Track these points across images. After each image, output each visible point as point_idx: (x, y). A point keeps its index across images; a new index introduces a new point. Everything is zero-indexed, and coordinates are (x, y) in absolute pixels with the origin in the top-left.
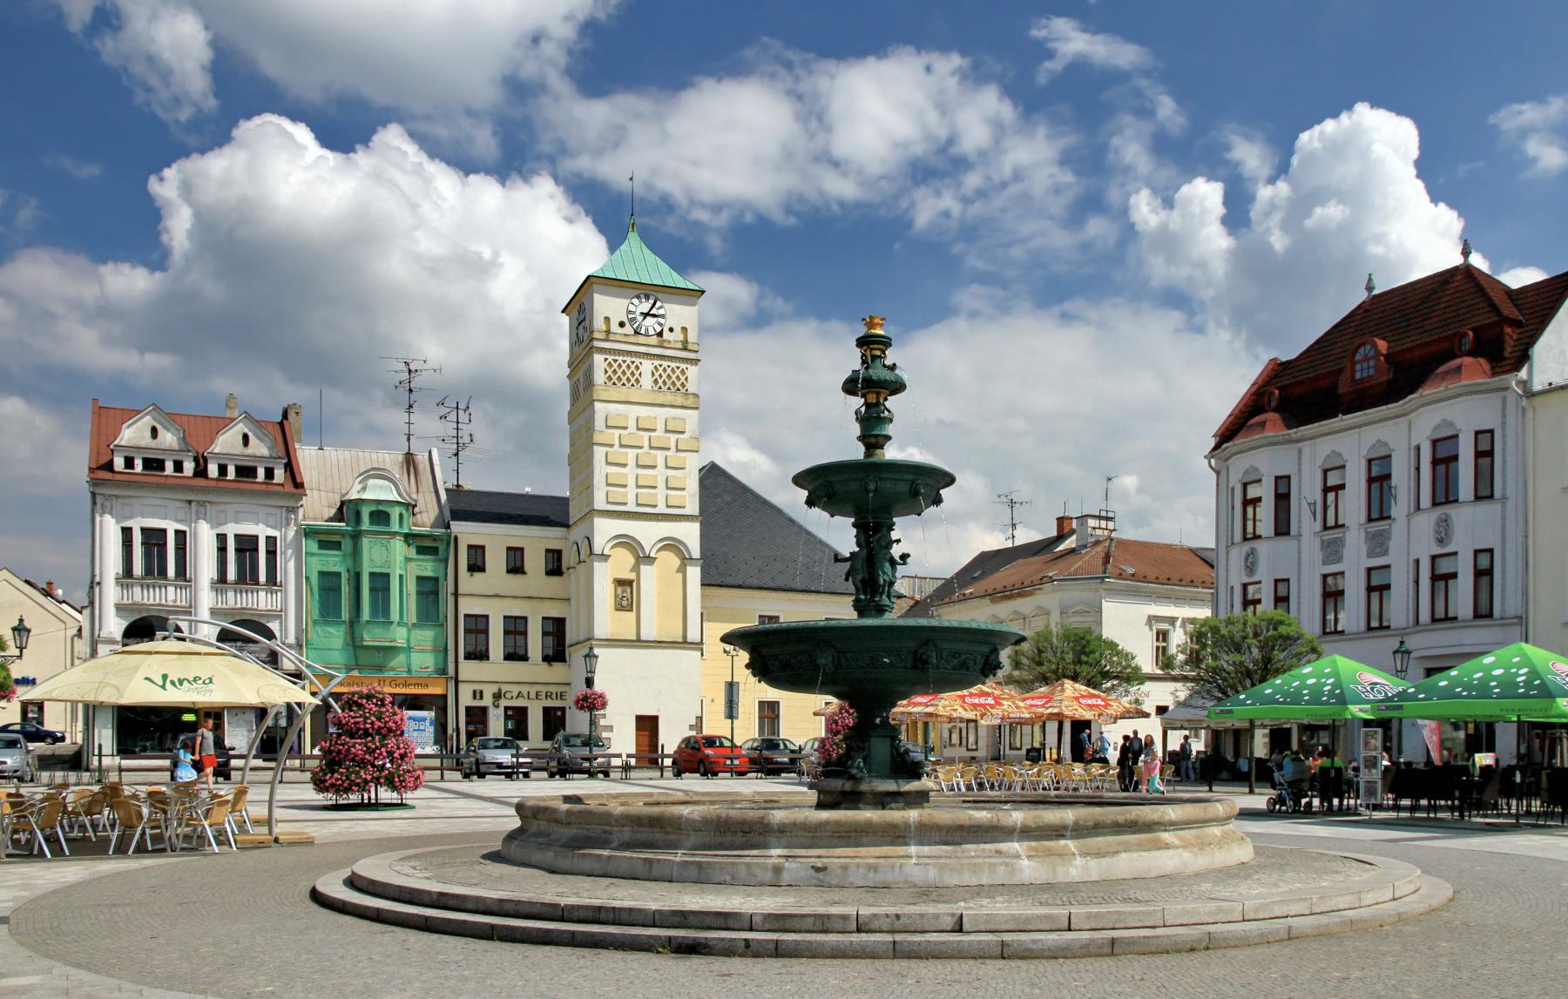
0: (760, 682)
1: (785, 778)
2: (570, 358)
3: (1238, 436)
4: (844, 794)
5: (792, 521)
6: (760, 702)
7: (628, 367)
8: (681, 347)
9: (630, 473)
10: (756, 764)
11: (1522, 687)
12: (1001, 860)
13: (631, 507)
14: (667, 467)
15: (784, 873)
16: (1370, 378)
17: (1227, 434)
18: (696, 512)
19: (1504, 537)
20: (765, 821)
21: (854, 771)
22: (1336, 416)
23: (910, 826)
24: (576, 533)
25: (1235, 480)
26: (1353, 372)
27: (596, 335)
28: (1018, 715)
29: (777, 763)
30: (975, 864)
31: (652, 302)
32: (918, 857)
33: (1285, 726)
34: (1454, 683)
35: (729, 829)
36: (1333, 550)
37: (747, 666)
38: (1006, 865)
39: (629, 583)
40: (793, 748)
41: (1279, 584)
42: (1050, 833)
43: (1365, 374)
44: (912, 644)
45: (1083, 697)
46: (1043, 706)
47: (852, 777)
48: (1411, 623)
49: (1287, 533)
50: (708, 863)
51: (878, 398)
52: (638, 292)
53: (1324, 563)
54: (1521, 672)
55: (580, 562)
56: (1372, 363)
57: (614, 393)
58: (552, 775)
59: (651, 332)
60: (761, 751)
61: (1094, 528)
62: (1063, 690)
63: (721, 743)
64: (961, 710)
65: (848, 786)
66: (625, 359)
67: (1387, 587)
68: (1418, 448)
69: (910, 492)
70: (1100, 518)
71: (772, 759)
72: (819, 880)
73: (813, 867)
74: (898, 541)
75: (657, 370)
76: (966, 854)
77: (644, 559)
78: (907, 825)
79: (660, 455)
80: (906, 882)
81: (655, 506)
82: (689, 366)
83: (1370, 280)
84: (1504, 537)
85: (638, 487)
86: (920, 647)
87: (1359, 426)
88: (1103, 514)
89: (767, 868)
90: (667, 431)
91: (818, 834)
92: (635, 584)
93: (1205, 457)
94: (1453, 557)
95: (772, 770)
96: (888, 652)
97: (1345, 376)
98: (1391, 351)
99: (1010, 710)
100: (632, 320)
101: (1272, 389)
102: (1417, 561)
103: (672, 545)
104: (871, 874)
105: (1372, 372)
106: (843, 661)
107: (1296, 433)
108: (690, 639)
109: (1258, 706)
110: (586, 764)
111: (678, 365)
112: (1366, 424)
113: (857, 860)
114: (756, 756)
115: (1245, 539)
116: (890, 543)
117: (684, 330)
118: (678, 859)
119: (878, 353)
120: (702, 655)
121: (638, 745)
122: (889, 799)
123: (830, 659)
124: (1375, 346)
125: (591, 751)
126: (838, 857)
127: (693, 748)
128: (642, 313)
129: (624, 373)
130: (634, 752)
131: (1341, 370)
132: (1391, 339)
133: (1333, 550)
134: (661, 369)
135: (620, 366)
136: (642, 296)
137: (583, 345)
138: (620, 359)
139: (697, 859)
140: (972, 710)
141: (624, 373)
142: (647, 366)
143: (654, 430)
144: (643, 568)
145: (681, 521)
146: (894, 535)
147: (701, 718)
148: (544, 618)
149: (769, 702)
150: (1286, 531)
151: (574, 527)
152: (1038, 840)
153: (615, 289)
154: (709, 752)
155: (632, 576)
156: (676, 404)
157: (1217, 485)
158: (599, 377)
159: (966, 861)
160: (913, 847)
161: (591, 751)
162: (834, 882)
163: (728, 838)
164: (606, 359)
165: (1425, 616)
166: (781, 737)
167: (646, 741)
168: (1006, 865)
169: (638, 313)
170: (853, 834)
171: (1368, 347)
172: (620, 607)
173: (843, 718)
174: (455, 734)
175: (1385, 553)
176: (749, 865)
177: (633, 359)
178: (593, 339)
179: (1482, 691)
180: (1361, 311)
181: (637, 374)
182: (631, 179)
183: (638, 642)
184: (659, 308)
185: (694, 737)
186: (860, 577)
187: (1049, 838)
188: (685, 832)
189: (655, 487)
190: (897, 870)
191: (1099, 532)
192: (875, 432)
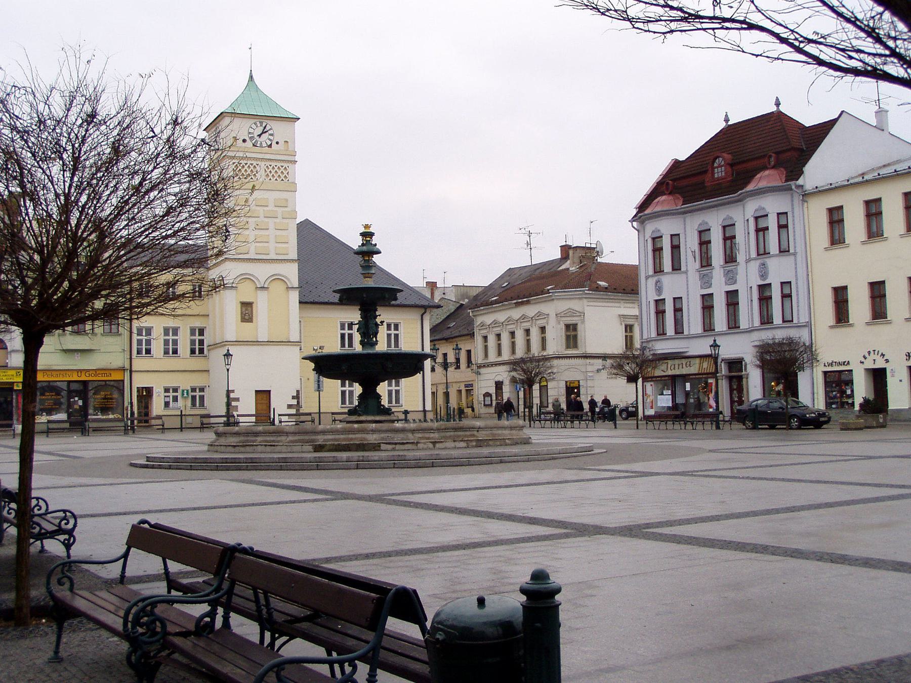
18: (296, 257)
19: (796, 276)
25: (648, 233)
26: (713, 174)
36: (706, 281)
37: (313, 370)
43: (720, 175)
83: (726, 115)
84: (796, 276)
100: (252, 138)
116: (376, 317)
130: (254, 413)
131: (706, 172)
133: (706, 281)
134: (271, 168)
146: (377, 313)
169: (256, 136)
171: (721, 159)
174: (129, 406)
180: (721, 134)
182: (250, 48)
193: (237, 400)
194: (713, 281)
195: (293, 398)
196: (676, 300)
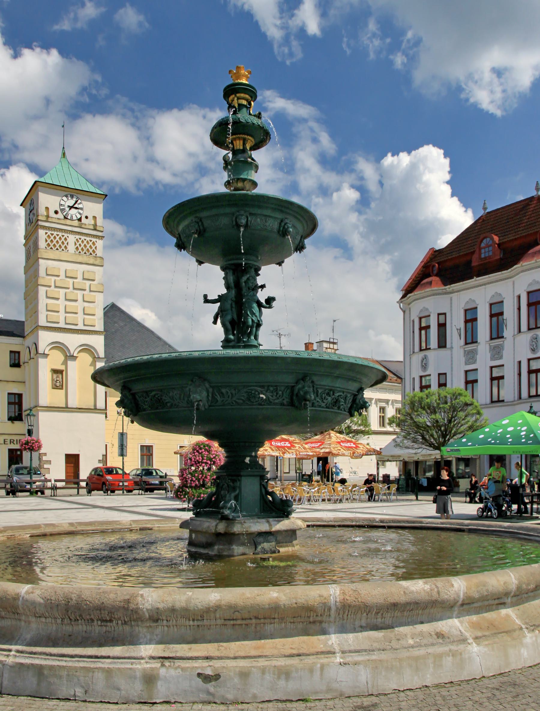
0: (132, 422)
1: (157, 494)
2: (26, 233)
3: (416, 290)
4: (218, 535)
5: (159, 338)
6: (141, 446)
7: (60, 238)
8: (93, 228)
9: (61, 304)
10: (138, 485)
11: (523, 438)
12: (446, 649)
13: (62, 325)
14: (84, 301)
15: (159, 683)
16: (489, 257)
17: (409, 289)
18: (102, 329)
20: (132, 606)
21: (227, 512)
22: (472, 278)
23: (330, 609)
24: (29, 341)
26: (480, 254)
27: (40, 218)
28: (305, 454)
29: (152, 484)
30: (417, 659)
31: (75, 199)
32: (343, 652)
33: (449, 459)
34: (488, 435)
35: (81, 616)
36: (471, 357)
38: (454, 654)
39: (61, 372)
40: (161, 474)
41: (441, 376)
42: (491, 602)
43: (487, 255)
44: (289, 379)
45: (342, 442)
46: (318, 447)
47: (225, 518)
48: (516, 398)
49: (445, 346)
50: (51, 668)
51: (244, 144)
52: (66, 193)
53: (466, 364)
54: (523, 429)
55: (31, 359)
56: (491, 248)
57: (52, 254)
58: (8, 493)
59: (75, 218)
60: (141, 476)
61: (327, 348)
62: (330, 437)
63: (117, 471)
64: (269, 450)
65: (222, 527)
66: (58, 233)
67: (476, 381)
68: (519, 297)
69: (279, 231)
70: (329, 342)
71: (148, 482)
72: (209, 693)
73: (199, 675)
74: (263, 287)
75: (78, 241)
76: (403, 642)
77: (70, 357)
78: (326, 607)
79: (80, 294)
80: (329, 690)
81: (77, 325)
82: (97, 240)
85: (66, 312)
86: (297, 382)
87: (485, 284)
88: (332, 340)
89: (135, 678)
90: (84, 279)
91: (205, 622)
92: (64, 373)
93: (397, 302)
94: (502, 367)
95: (149, 489)
96: (265, 387)
97: (475, 257)
98: (501, 242)
99: (300, 450)
100: (63, 210)
101: (433, 263)
102: (520, 362)
103: (87, 349)
104: (282, 683)
105: (491, 254)
106: (218, 398)
107: (449, 288)
108: (98, 407)
109: (477, 446)
110: (28, 487)
111: (91, 239)
112: (489, 283)
113: (262, 663)
114: (138, 480)
115: (421, 350)
116: (256, 288)
117: (95, 218)
118: (10, 660)
119: (244, 102)
120: (106, 417)
121: (67, 472)
122: (261, 539)
123: (205, 394)
124: (492, 239)
125: (31, 478)
126: (235, 658)
127: (99, 475)
128: (69, 206)
129: (57, 242)
131: (473, 253)
132: (500, 235)
133: (471, 357)
134: (80, 241)
135: (55, 238)
136: (69, 196)
137: (33, 224)
138: (55, 233)
139: (37, 662)
140: (277, 450)
141: (57, 242)
142: (72, 238)
143: (76, 278)
144: (69, 363)
145: (92, 334)
147: (106, 455)
148: (9, 394)
149: (146, 446)
150: (444, 345)
151: (27, 337)
152: (478, 613)
153: (52, 191)
154: (109, 477)
155: (62, 368)
156: (89, 263)
157: (404, 319)
158: (42, 244)
159: (404, 654)
160: (333, 637)
161: (31, 478)
162: (230, 696)
163: (81, 628)
164: (46, 233)
165: (525, 394)
166: (154, 467)
167: (72, 470)
168: (454, 654)
170: (254, 621)
171: (488, 239)
172: (55, 387)
173: (195, 456)
175: (501, 358)
176: (108, 672)
177: (63, 234)
178: (38, 220)
179: (503, 441)
180: (481, 221)
181: (66, 243)
183: (66, 409)
184: (79, 204)
185: (100, 468)
186: (229, 317)
187: (489, 608)
188: (23, 618)
189: (76, 313)
190: (317, 674)
191: (329, 350)
192: (242, 177)
193: (49, 462)
194: (478, 357)
195: (99, 461)
196: (441, 376)
